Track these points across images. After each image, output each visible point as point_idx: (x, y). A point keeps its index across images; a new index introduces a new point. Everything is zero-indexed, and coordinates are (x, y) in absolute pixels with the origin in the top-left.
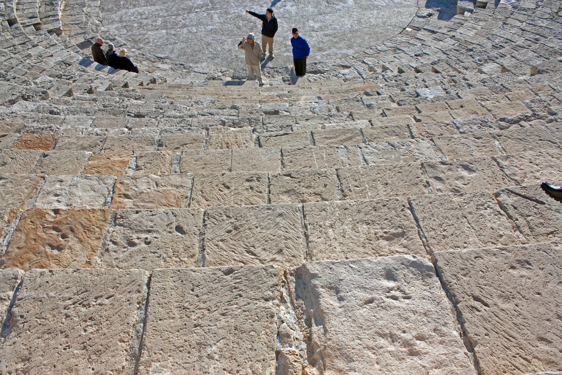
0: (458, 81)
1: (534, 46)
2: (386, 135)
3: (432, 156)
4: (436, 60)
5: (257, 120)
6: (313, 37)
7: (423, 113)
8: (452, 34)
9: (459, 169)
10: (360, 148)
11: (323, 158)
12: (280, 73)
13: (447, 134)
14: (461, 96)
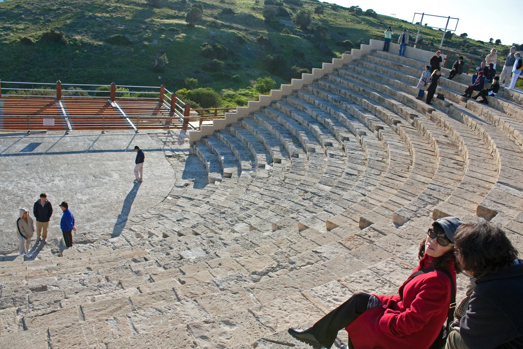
0: (215, 241)
1: (272, 207)
2: (153, 300)
3: (197, 316)
4: (196, 223)
5: (22, 299)
6: (81, 209)
7: (187, 273)
8: (207, 200)
9: (221, 325)
10: (130, 317)
11: (92, 333)
12: (49, 245)
13: (210, 293)
14: (219, 255)
